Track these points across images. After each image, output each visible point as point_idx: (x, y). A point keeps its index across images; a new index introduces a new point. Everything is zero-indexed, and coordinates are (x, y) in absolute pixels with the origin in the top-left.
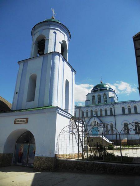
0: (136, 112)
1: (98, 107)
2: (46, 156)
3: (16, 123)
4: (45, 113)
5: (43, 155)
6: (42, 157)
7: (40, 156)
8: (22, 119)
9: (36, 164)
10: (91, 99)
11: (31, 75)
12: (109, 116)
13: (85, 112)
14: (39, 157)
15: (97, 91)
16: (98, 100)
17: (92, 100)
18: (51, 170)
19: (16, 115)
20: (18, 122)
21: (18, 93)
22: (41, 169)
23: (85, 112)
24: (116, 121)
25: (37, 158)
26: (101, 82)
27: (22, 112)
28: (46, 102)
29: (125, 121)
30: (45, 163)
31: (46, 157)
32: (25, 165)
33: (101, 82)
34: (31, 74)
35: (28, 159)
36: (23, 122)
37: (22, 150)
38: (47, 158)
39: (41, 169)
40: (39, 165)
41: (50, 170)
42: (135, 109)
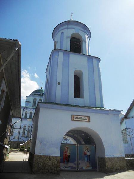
0: (30, 118)
1: (29, 110)
2: (117, 157)
3: (75, 119)
4: (108, 114)
5: (114, 156)
6: (113, 158)
7: (111, 157)
8: (83, 117)
9: (108, 166)
10: (32, 101)
11: (75, 70)
12: (27, 119)
13: (29, 112)
14: (110, 158)
15: (39, 95)
16: (33, 103)
17: (33, 103)
18: (124, 169)
19: (74, 111)
20: (76, 119)
21: (57, 83)
22: (114, 170)
23: (29, 112)
24: (20, 125)
25: (108, 159)
26: (42, 88)
27: (87, 109)
28: (98, 104)
29: (26, 124)
30: (117, 163)
31: (118, 157)
32: (75, 169)
33: (42, 88)
34: (76, 70)
35: (78, 162)
36: (83, 120)
37: (68, 152)
38: (118, 158)
39: (114, 170)
40: (112, 166)
41: (123, 169)
42: (31, 115)
